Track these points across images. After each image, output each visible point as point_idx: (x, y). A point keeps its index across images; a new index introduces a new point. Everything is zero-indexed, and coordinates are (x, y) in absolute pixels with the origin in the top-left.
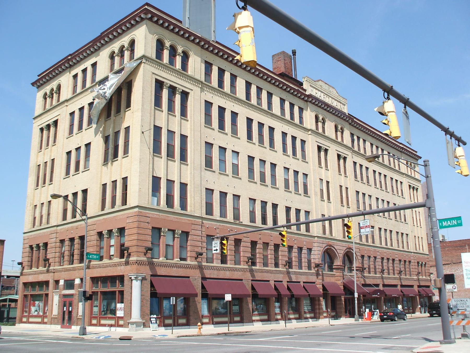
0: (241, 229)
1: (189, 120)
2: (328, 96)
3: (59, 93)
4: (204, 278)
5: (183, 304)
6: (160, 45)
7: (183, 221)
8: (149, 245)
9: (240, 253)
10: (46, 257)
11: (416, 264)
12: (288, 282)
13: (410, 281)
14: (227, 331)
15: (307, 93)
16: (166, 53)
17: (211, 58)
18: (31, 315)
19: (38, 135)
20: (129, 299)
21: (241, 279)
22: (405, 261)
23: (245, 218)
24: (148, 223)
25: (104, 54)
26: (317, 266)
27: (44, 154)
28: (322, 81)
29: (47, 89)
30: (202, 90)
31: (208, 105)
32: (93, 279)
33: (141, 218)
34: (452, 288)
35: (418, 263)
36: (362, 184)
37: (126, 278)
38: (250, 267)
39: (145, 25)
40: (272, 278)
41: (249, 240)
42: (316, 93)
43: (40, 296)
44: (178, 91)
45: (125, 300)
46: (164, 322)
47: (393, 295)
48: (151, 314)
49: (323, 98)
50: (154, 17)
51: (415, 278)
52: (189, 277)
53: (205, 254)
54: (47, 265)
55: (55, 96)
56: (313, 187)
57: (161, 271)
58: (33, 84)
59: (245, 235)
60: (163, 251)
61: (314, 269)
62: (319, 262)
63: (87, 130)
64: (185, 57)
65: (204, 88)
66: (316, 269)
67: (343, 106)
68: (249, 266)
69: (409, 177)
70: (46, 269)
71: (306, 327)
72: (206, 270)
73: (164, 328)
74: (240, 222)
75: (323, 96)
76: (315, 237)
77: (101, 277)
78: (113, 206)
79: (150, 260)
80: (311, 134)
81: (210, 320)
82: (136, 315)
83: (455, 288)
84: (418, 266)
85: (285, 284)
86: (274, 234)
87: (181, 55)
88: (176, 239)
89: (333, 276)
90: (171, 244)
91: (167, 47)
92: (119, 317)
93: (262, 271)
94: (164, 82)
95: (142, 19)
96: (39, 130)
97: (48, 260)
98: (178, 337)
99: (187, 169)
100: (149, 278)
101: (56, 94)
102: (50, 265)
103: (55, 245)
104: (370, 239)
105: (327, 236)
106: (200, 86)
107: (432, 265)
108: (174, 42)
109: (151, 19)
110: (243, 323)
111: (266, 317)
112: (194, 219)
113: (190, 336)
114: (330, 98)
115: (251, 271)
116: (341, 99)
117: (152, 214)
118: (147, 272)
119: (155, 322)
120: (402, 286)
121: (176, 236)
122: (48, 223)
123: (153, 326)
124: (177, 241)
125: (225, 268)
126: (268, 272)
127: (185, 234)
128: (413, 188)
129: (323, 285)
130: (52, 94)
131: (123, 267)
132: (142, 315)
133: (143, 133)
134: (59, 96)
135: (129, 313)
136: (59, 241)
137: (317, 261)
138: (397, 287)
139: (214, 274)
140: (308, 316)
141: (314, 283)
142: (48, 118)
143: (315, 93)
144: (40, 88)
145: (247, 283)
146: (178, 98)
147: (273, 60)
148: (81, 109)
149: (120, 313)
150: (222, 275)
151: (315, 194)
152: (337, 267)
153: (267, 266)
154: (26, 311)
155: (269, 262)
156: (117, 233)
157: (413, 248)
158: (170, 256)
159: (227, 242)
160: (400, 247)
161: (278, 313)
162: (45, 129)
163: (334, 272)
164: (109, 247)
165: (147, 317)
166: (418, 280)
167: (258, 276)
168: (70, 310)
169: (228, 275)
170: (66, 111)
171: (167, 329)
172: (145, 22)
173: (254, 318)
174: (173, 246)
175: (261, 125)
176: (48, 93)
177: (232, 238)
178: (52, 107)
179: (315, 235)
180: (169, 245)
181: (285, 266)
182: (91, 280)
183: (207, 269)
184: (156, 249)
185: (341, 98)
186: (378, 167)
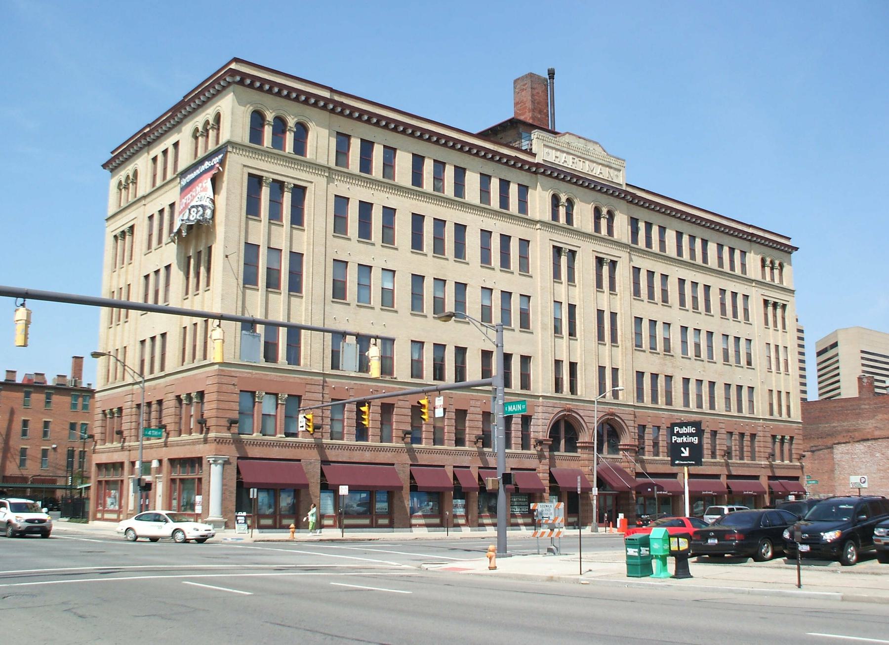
0: (393, 388)
1: (306, 229)
2: (584, 158)
3: (218, 129)
4: (325, 462)
5: (290, 498)
6: (258, 120)
7: (291, 380)
8: (235, 415)
9: (391, 425)
10: (160, 422)
11: (770, 440)
12: (480, 468)
13: (751, 469)
14: (340, 537)
15: (537, 160)
16: (268, 131)
17: (346, 125)
18: (106, 509)
19: (112, 246)
20: (207, 490)
21: (392, 462)
22: (742, 435)
23: (402, 370)
24: (234, 385)
25: (187, 129)
26: (540, 442)
27: (119, 275)
28: (570, 134)
29: (122, 175)
30: (330, 180)
31: (341, 202)
32: (172, 461)
33: (222, 379)
34: (859, 481)
35: (774, 437)
36: (650, 304)
37: (204, 462)
38: (409, 446)
39: (232, 93)
40: (449, 463)
41: (408, 404)
42: (557, 157)
43: (115, 482)
44: (287, 187)
45: (203, 491)
46: (258, 522)
47: (745, 493)
48: (237, 511)
49: (571, 164)
50: (245, 79)
51: (764, 462)
52: (299, 460)
53: (329, 426)
54: (205, 429)
55: (212, 133)
56: (540, 316)
57: (253, 452)
58: (105, 166)
59: (401, 397)
60: (258, 424)
61: (535, 447)
62: (543, 436)
63: (167, 245)
64: (302, 131)
65: (334, 176)
66: (539, 448)
67: (616, 173)
68: (406, 443)
69: (765, 286)
70: (202, 436)
71: (483, 536)
72: (330, 451)
73: (257, 530)
74: (392, 378)
75: (571, 160)
76: (539, 397)
77: (180, 459)
78: (152, 372)
79: (236, 436)
80: (540, 229)
81: (335, 522)
82: (215, 512)
83: (864, 482)
84: (774, 442)
85: (475, 473)
86: (456, 394)
87: (293, 131)
88: (279, 406)
89: (577, 459)
90: (273, 413)
91: (268, 121)
92: (197, 514)
93: (430, 452)
94: (262, 177)
95: (229, 84)
96: (112, 239)
97: (205, 422)
98: (255, 541)
99: (301, 303)
100: (234, 462)
101: (133, 185)
102: (208, 429)
103: (131, 412)
104: (662, 397)
105: (566, 395)
106: (327, 174)
107: (880, 435)
108: (282, 112)
109: (241, 83)
110: (393, 528)
111: (437, 521)
112: (310, 377)
113: (274, 541)
114: (587, 162)
115: (411, 452)
116: (612, 160)
117: (240, 372)
118: (232, 452)
119: (243, 522)
120: (730, 477)
121: (280, 402)
122: (162, 368)
123: (240, 526)
124: (281, 411)
125: (362, 447)
126: (441, 452)
127: (297, 399)
128: (775, 305)
129: (551, 474)
130: (207, 131)
131: (201, 446)
132: (224, 512)
133: (227, 256)
134: (218, 134)
135: (207, 508)
136: (135, 406)
137: (541, 436)
138: (719, 479)
139: (344, 456)
140: (520, 521)
141: (535, 470)
142: (121, 223)
143: (554, 157)
144: (113, 172)
145: (401, 469)
146: (287, 198)
147: (515, 88)
148: (161, 212)
149: (198, 509)
150: (357, 456)
151: (542, 328)
152: (583, 445)
153: (442, 444)
154: (101, 504)
155: (446, 438)
156: (196, 397)
157: (762, 411)
158: (270, 428)
159: (369, 409)
160: (732, 410)
161: (462, 516)
162: (120, 238)
163: (579, 453)
164: (189, 418)
165: (230, 515)
166: (771, 467)
167: (423, 459)
168: (147, 503)
169: (368, 456)
170: (144, 212)
171: (262, 532)
172: (231, 88)
173: (414, 521)
174: (275, 416)
175: (440, 224)
176: (200, 129)
177: (378, 402)
178: (155, 188)
179: (540, 394)
180: (269, 415)
181: (475, 444)
182: (169, 463)
183: (331, 449)
184: (248, 421)
185: (612, 158)
186: (692, 272)
